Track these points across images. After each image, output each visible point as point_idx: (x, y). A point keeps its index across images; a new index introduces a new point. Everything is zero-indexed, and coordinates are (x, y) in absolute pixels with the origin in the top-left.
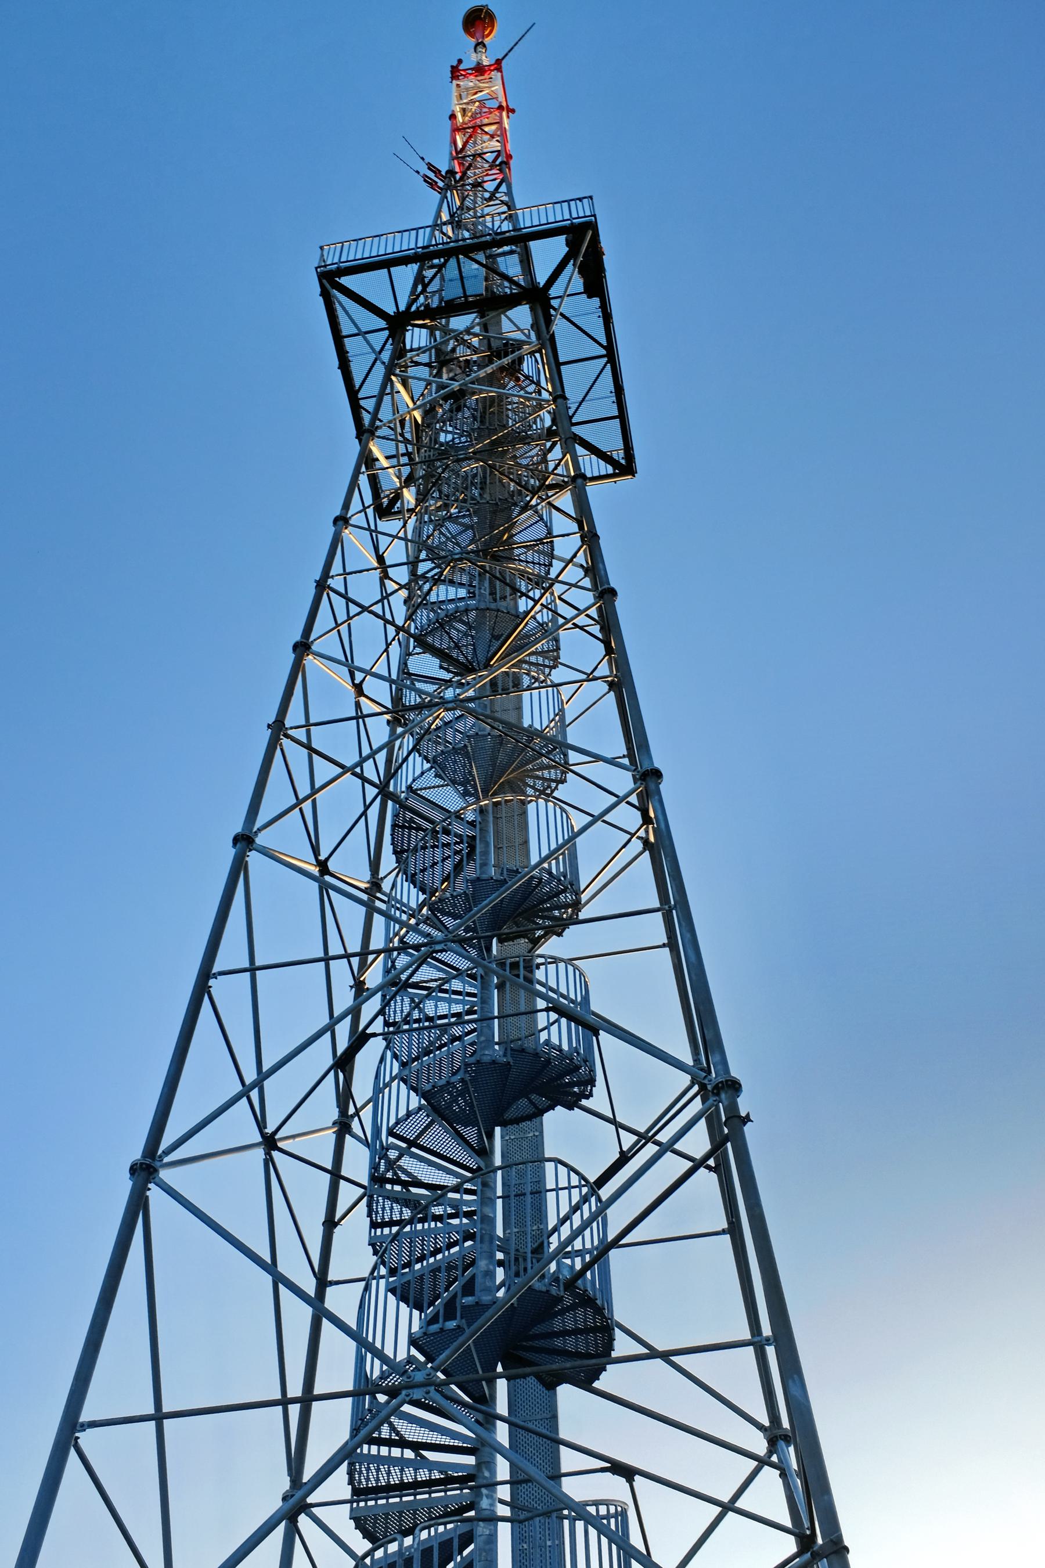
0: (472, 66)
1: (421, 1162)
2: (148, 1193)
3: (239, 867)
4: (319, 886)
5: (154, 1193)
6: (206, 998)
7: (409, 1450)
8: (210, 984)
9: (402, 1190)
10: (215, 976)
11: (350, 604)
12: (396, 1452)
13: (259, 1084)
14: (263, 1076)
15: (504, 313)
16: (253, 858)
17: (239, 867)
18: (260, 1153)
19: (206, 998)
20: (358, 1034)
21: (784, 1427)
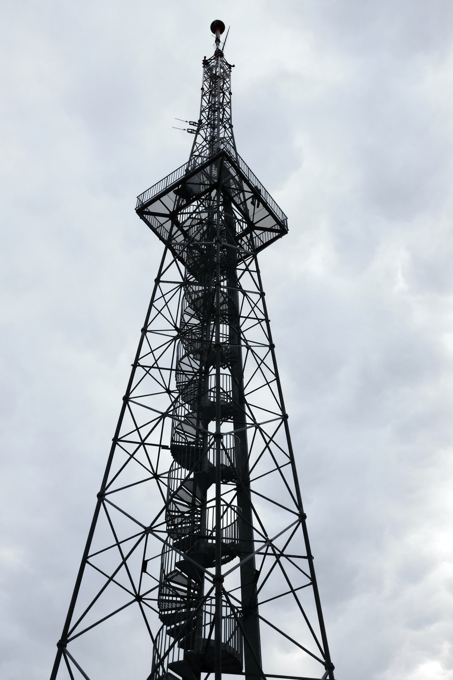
0: (213, 55)
1: (183, 506)
2: (299, 511)
3: (270, 339)
4: (248, 267)
5: (280, 413)
6: (310, 576)
7: (190, 476)
8: (265, 317)
9: (181, 600)
10: (275, 380)
11: (256, 318)
12: (174, 599)
13: (267, 444)
14: (267, 446)
15: (155, 228)
16: (268, 343)
17: (270, 339)
18: (270, 537)
19: (310, 576)
20: (227, 594)
21: (220, 210)
